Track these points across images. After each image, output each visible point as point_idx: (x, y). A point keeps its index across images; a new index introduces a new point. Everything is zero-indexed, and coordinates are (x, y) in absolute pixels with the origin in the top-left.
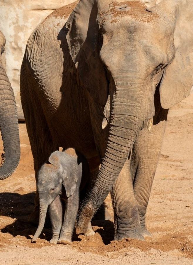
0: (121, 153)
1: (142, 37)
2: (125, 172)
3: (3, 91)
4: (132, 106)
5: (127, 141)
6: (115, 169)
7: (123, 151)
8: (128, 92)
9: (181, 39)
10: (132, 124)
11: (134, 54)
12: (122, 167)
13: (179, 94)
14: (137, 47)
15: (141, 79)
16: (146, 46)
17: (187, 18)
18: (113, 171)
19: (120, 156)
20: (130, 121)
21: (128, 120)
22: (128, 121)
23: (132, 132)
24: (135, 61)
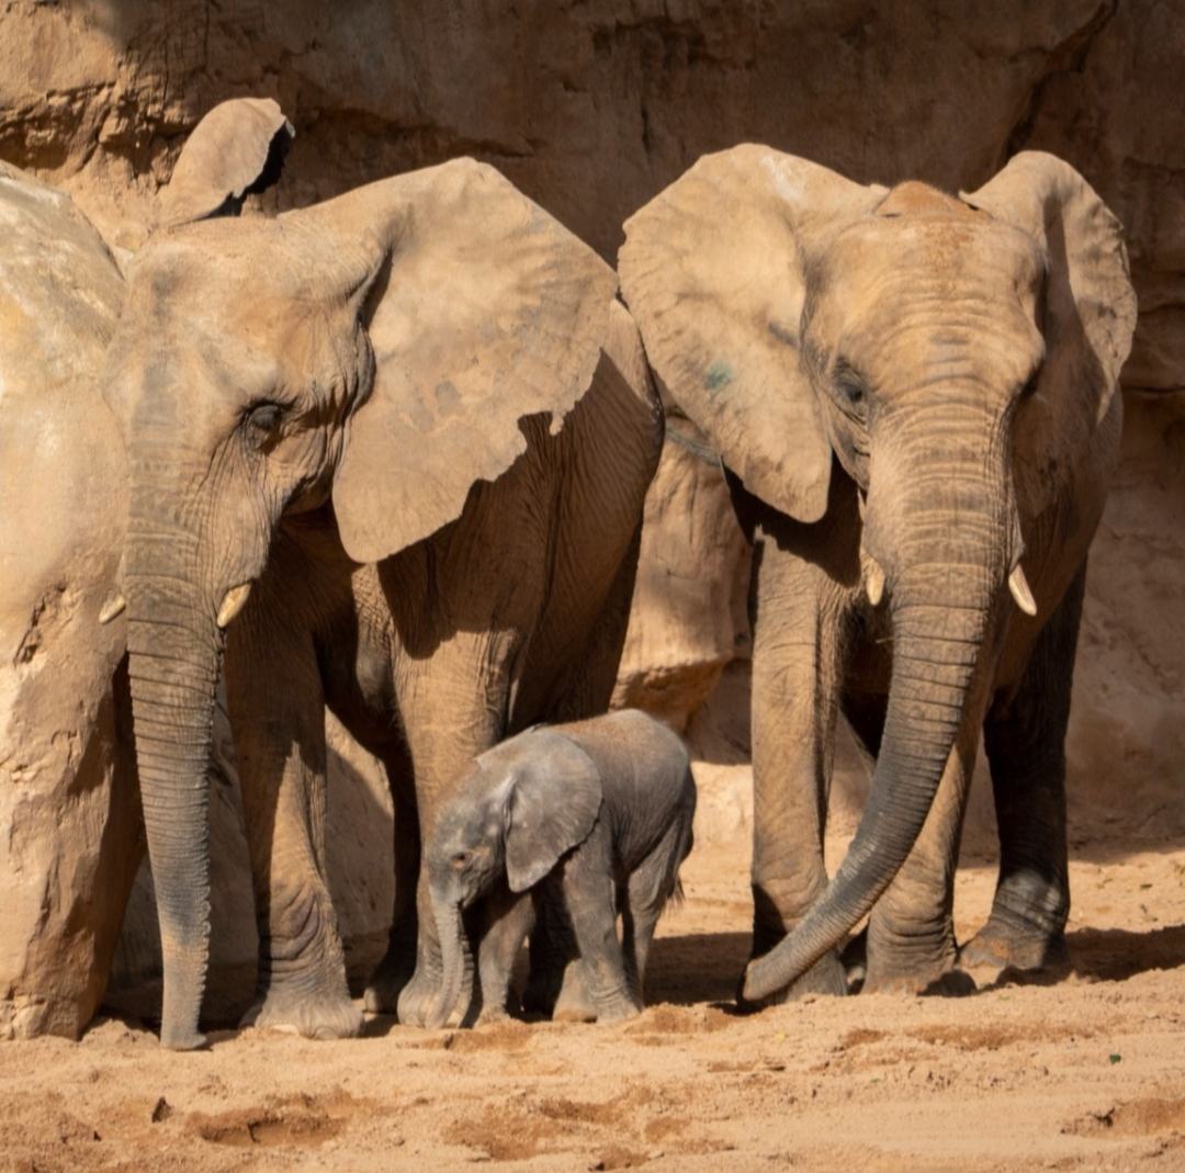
0: (162, 710)
1: (194, 308)
2: (75, 753)
3: (935, 670)
4: (162, 541)
5: (171, 664)
6: (163, 766)
7: (167, 700)
8: (152, 495)
9: (415, 322)
10: (172, 607)
11: (170, 367)
12: (993, 923)
13: (417, 510)
14: (178, 343)
15: (196, 449)
16: (204, 338)
17: (462, 249)
18: (163, 776)
19: (162, 718)
20: (164, 594)
21: (159, 592)
22: (156, 597)
23: (181, 634)
24: (169, 390)
